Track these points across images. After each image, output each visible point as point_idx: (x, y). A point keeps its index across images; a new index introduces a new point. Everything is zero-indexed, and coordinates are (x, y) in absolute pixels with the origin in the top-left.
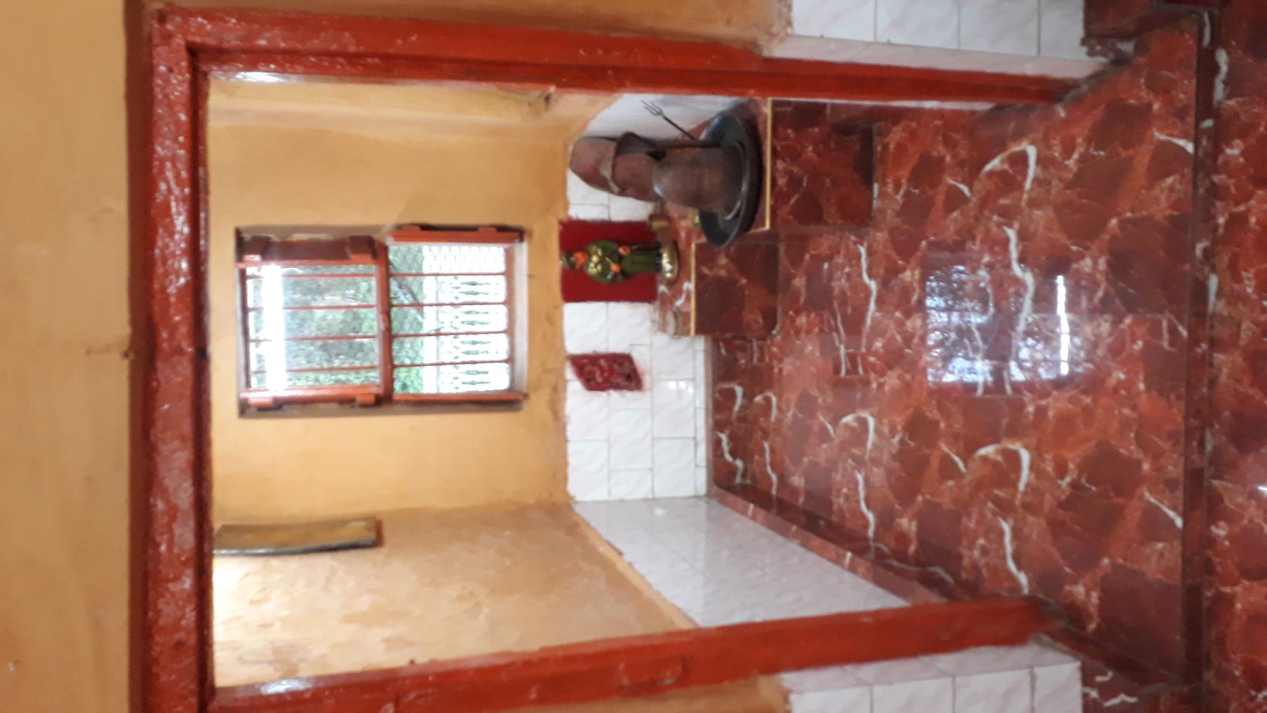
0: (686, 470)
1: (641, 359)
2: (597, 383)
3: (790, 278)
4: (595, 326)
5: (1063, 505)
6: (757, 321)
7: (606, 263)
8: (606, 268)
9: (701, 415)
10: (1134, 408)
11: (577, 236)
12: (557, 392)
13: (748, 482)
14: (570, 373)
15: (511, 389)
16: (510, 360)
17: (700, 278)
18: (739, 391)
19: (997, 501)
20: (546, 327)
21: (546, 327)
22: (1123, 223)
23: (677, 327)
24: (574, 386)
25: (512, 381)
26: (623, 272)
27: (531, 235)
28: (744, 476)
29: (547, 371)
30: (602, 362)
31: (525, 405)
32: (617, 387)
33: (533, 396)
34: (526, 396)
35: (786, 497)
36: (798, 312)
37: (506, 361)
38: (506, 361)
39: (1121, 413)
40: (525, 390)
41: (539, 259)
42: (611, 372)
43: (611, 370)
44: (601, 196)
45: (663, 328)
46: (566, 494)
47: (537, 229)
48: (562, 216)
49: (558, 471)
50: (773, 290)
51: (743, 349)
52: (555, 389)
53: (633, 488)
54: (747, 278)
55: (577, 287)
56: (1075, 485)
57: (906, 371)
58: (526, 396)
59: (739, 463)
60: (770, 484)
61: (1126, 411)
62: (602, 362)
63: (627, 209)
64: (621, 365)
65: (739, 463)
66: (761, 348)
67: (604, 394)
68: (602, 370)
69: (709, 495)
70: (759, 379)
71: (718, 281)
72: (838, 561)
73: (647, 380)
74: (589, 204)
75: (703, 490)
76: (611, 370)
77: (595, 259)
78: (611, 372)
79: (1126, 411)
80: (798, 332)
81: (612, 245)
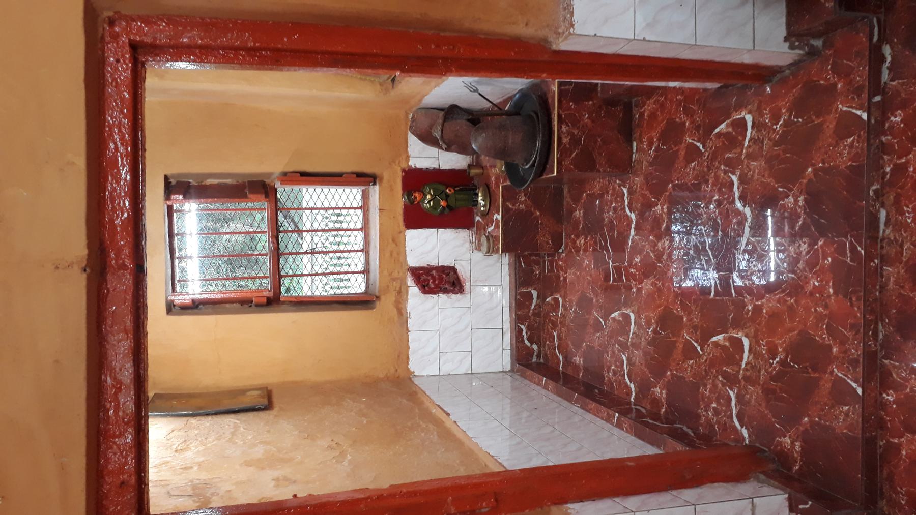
0: (496, 352)
1: (463, 270)
2: (430, 288)
3: (571, 211)
4: (428, 246)
5: (773, 378)
6: (548, 243)
7: (435, 200)
8: (437, 204)
9: (507, 311)
10: (826, 307)
11: (415, 180)
12: (401, 295)
13: (542, 361)
14: (410, 281)
15: (366, 292)
16: (366, 271)
17: (506, 211)
18: (535, 293)
19: (725, 375)
20: (393, 247)
21: (393, 247)
22: (815, 171)
23: (489, 247)
24: (414, 290)
25: (367, 287)
26: (448, 206)
27: (381, 180)
28: (538, 356)
29: (394, 279)
30: (434, 272)
31: (377, 303)
32: (446, 291)
33: (383, 298)
34: (378, 298)
35: (570, 372)
36: (578, 237)
37: (363, 272)
38: (363, 272)
39: (816, 310)
40: (377, 294)
41: (387, 197)
42: (441, 280)
43: (441, 279)
44: (434, 151)
45: (478, 248)
46: (408, 369)
47: (386, 176)
48: (404, 165)
49: (403, 355)
50: (559, 220)
51: (538, 263)
52: (399, 292)
53: (456, 365)
54: (540, 211)
55: (416, 218)
56: (782, 363)
57: (658, 280)
58: (378, 298)
59: (535, 347)
60: (629, 393)
61: (820, 309)
62: (434, 272)
63: (452, 161)
64: (448, 274)
65: (535, 347)
66: (551, 262)
67: (435, 296)
68: (433, 277)
69: (512, 370)
70: (550, 285)
71: (519, 213)
72: (609, 420)
73: (467, 286)
74: (423, 156)
75: (508, 367)
76: (441, 279)
77: (428, 197)
78: (441, 280)
79: (820, 309)
80: (578, 250)
81: (442, 187)
